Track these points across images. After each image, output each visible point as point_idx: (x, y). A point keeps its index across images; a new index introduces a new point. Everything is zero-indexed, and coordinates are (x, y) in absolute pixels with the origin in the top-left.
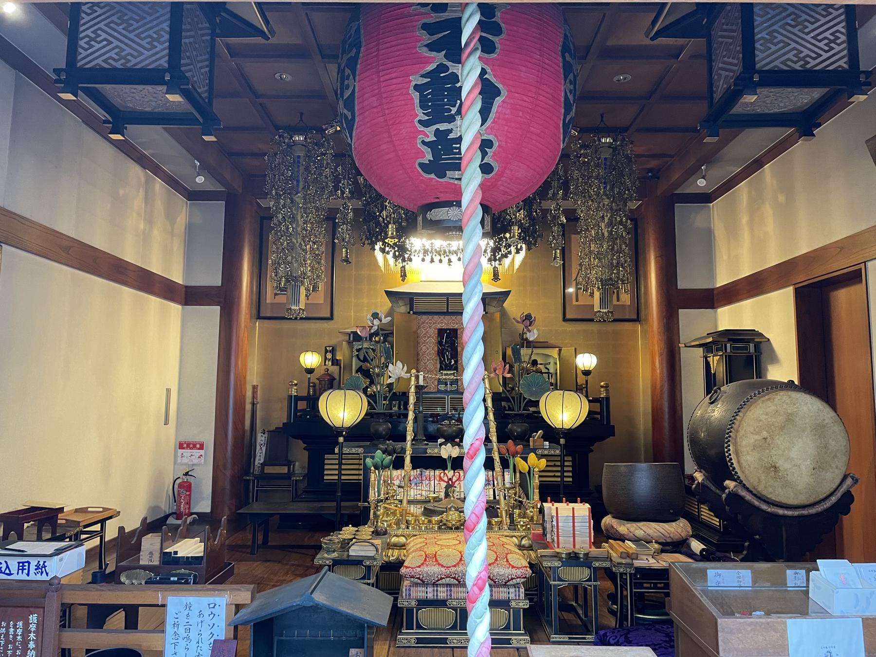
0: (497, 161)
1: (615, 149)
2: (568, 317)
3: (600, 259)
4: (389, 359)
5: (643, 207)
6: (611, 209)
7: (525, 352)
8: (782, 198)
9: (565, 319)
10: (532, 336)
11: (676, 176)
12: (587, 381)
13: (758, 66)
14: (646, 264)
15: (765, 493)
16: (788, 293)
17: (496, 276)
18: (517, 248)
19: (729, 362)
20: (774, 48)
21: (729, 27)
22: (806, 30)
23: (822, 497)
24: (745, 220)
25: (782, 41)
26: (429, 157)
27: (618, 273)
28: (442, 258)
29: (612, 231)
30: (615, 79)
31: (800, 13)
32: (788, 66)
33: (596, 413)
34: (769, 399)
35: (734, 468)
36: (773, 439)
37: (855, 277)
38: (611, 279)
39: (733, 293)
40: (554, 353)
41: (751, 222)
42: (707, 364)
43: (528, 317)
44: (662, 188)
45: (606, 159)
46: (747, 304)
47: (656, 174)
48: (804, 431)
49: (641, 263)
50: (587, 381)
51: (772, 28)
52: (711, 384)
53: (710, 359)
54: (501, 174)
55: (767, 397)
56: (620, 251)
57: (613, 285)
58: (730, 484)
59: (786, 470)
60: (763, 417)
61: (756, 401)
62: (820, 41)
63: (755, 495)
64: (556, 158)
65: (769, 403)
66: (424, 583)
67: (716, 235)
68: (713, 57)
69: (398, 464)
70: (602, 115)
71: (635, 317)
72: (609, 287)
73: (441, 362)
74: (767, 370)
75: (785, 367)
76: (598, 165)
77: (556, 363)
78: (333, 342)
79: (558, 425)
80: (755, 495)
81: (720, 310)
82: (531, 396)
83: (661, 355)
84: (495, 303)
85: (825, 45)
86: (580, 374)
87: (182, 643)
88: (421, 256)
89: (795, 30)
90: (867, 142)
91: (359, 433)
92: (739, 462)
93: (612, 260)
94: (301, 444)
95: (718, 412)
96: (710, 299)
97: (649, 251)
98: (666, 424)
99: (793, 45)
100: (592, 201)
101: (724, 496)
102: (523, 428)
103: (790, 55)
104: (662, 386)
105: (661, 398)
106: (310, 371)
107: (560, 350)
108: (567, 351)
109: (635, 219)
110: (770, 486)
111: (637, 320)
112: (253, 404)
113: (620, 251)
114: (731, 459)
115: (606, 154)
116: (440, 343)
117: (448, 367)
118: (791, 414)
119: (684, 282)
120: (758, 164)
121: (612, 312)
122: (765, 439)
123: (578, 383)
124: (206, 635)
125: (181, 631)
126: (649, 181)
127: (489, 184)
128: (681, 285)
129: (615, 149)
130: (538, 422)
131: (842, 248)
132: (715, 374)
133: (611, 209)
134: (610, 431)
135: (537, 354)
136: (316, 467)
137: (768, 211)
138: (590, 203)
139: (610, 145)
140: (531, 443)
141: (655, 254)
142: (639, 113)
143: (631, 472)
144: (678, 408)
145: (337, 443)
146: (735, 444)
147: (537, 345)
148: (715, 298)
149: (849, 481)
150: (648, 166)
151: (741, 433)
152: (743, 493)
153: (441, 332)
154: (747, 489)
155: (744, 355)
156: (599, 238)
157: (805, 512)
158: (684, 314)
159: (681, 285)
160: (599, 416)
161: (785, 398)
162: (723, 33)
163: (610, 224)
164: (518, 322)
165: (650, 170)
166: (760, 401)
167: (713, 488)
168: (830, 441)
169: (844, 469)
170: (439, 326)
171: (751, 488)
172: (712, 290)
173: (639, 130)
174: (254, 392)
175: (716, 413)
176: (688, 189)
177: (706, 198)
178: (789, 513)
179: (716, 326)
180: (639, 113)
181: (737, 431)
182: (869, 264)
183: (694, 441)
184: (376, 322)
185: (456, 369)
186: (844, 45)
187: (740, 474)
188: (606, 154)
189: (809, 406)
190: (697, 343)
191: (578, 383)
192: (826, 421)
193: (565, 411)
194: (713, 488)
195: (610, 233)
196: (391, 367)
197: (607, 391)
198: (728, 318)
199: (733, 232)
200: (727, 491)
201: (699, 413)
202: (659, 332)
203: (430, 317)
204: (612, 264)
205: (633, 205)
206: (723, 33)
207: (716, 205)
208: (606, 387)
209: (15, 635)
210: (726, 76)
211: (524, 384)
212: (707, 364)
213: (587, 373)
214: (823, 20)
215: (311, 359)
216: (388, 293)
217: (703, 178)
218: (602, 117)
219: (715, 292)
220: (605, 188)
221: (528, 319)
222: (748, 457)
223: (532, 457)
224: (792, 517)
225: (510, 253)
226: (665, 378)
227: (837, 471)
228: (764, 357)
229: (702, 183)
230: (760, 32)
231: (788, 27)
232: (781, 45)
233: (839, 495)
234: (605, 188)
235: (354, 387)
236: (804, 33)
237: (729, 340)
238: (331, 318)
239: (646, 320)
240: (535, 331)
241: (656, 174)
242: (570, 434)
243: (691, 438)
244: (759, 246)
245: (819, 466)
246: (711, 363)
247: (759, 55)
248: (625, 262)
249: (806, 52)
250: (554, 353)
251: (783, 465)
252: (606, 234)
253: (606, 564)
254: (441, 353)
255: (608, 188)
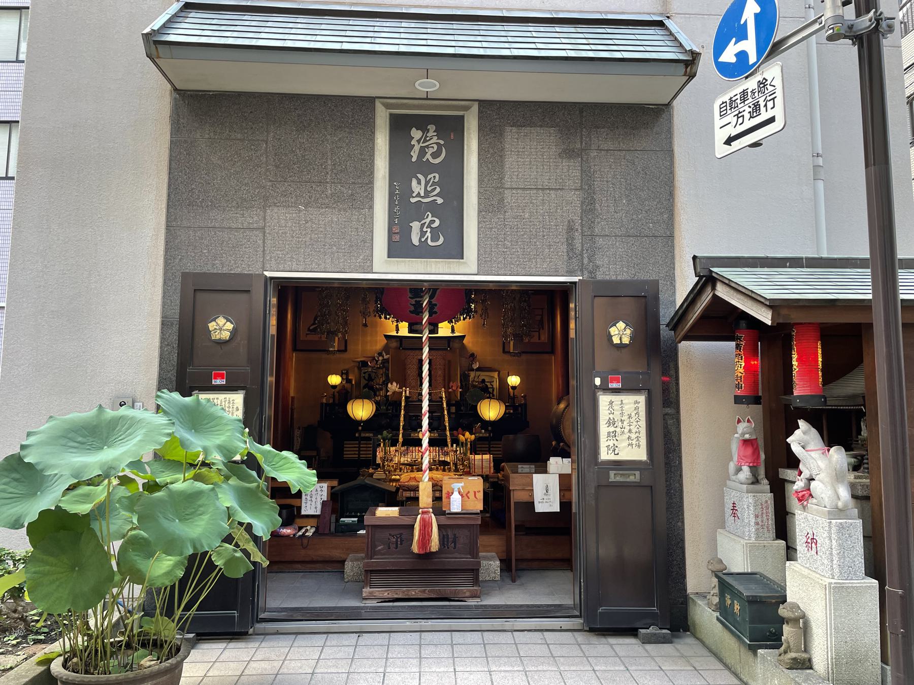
4: (388, 381)
26: (412, 308)
40: (496, 375)
66: (410, 490)
69: (394, 443)
78: (346, 367)
79: (487, 419)
87: (309, 503)
91: (368, 424)
94: (328, 435)
106: (334, 387)
112: (292, 410)
123: (504, 395)
124: (319, 499)
125: (308, 498)
135: (483, 375)
136: (338, 450)
145: (358, 430)
174: (292, 401)
184: (381, 358)
196: (389, 385)
197: (525, 400)
208: (524, 397)
209: (16, 638)
213: (514, 388)
215: (335, 380)
216: (385, 336)
223: (467, 434)
235: (369, 398)
238: (345, 350)
242: (490, 423)
250: (496, 375)
253: (496, 480)
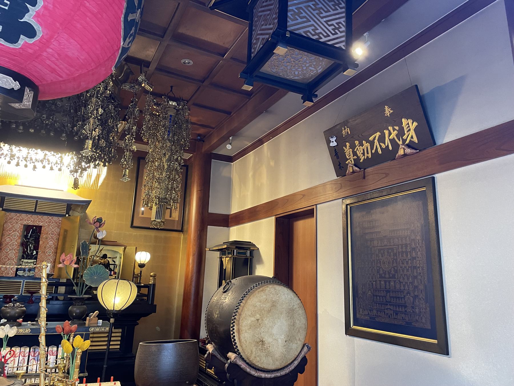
0: (41, 25)
1: (178, 110)
2: (134, 225)
3: (159, 183)
5: (193, 158)
6: (172, 150)
7: (94, 248)
8: (272, 163)
9: (132, 226)
10: (101, 236)
11: (215, 140)
12: (141, 272)
13: (288, 29)
14: (191, 195)
15: (254, 362)
16: (272, 220)
17: (76, 185)
18: (95, 164)
19: (235, 262)
20: (300, 20)
21: (268, 3)
22: (321, 15)
23: (289, 362)
24: (250, 174)
25: (305, 17)
27: (171, 194)
28: (28, 163)
29: (170, 165)
30: (183, 61)
31: (311, 20)
32: (307, 35)
33: (145, 295)
34: (262, 290)
35: (236, 343)
36: (262, 320)
37: (310, 213)
38: (166, 198)
39: (240, 218)
41: (254, 176)
42: (222, 262)
43: (99, 220)
44: (205, 148)
45: (171, 116)
46: (248, 226)
47: (201, 139)
48: (281, 314)
49: (187, 195)
50: (141, 272)
51: (300, 6)
52: (222, 275)
53: (223, 260)
54: (45, 43)
55: (261, 289)
56: (174, 180)
57: (167, 203)
58: (232, 356)
59: (269, 343)
60: (258, 304)
61: (254, 291)
62: (330, 26)
63: (247, 364)
64: (114, 54)
65: (262, 294)
67: (234, 181)
68: (254, 28)
70: (172, 87)
71: (180, 229)
72: (163, 204)
73: (24, 252)
74: (256, 268)
75: (265, 268)
76: (165, 118)
77: (121, 258)
80: (247, 364)
81: (232, 228)
82: (92, 283)
83: (194, 255)
84: (79, 209)
85: (333, 29)
86: (137, 265)
88: (8, 159)
89: (315, 13)
90: (324, 132)
92: (239, 338)
93: (168, 185)
95: (227, 300)
96: (226, 221)
97: (193, 186)
98: (192, 303)
99: (312, 22)
100: (159, 142)
101: (227, 365)
102: (82, 310)
103: (310, 29)
104: (192, 276)
105: (191, 285)
107: (125, 248)
108: (130, 249)
109: (186, 167)
110: (258, 356)
111: (181, 231)
113: (174, 180)
114: (234, 336)
115: (172, 113)
116: (26, 237)
117: (30, 256)
118: (274, 302)
119: (212, 209)
120: (260, 142)
121: (163, 222)
122: (258, 320)
123: (131, 274)
126: (197, 143)
127: (30, 51)
128: (211, 210)
129: (178, 110)
130: (93, 303)
131: (304, 195)
132: (225, 269)
133: (172, 150)
134: (153, 309)
135: (106, 250)
137: (264, 170)
138: (157, 143)
139: (175, 108)
140: (87, 322)
141: (197, 189)
142: (196, 92)
143: (160, 351)
144: (201, 292)
146: (238, 325)
147: (107, 243)
148: (230, 220)
149: (306, 349)
150: (198, 132)
151: (243, 315)
152: (240, 363)
153: (27, 228)
154: (243, 359)
155: (243, 257)
156: (160, 168)
157: (278, 374)
158: (211, 229)
159: (211, 210)
160: (146, 298)
161: (272, 290)
162: (263, 9)
163: (169, 160)
164: (91, 224)
165: (199, 135)
166: (257, 292)
167: (219, 356)
168: (297, 321)
169: (303, 341)
170: (25, 223)
171: (245, 359)
172: (228, 216)
173: (194, 104)
175: (227, 299)
176: (220, 151)
177: (230, 159)
178: (268, 376)
179: (228, 239)
180: (196, 92)
181: (240, 315)
182: (318, 206)
183: (209, 321)
185: (36, 258)
186: (344, 34)
187: (239, 348)
188: (172, 113)
189: (283, 293)
190: (217, 248)
191: (131, 274)
192: (295, 307)
193: (117, 296)
194: (219, 356)
195: (169, 166)
197: (155, 279)
198: (237, 233)
199: (243, 181)
200: (229, 361)
201: (215, 299)
202: (194, 240)
203: (18, 215)
204: (167, 187)
205: (187, 156)
206: (263, 9)
207: (235, 164)
208: (154, 276)
210: (263, 39)
211: (87, 273)
212: (222, 262)
213: (142, 266)
214: (332, 12)
217: (230, 144)
218: (172, 88)
219: (230, 217)
220: (169, 135)
221: (99, 221)
222: (246, 335)
224: (270, 379)
225: (89, 167)
226: (195, 271)
227: (299, 342)
228: (254, 260)
229: (229, 147)
230: (292, 5)
231: (310, 9)
232: (305, 19)
233: (299, 359)
234: (169, 135)
236: (320, 16)
237: (237, 247)
239: (187, 231)
240: (104, 232)
241: (201, 139)
243: (208, 318)
244: (257, 190)
245: (290, 339)
246: (224, 262)
247: (290, 22)
248: (177, 187)
249: (320, 30)
250: (121, 250)
251: (268, 339)
252: (166, 167)
254: (24, 245)
255: (171, 135)
